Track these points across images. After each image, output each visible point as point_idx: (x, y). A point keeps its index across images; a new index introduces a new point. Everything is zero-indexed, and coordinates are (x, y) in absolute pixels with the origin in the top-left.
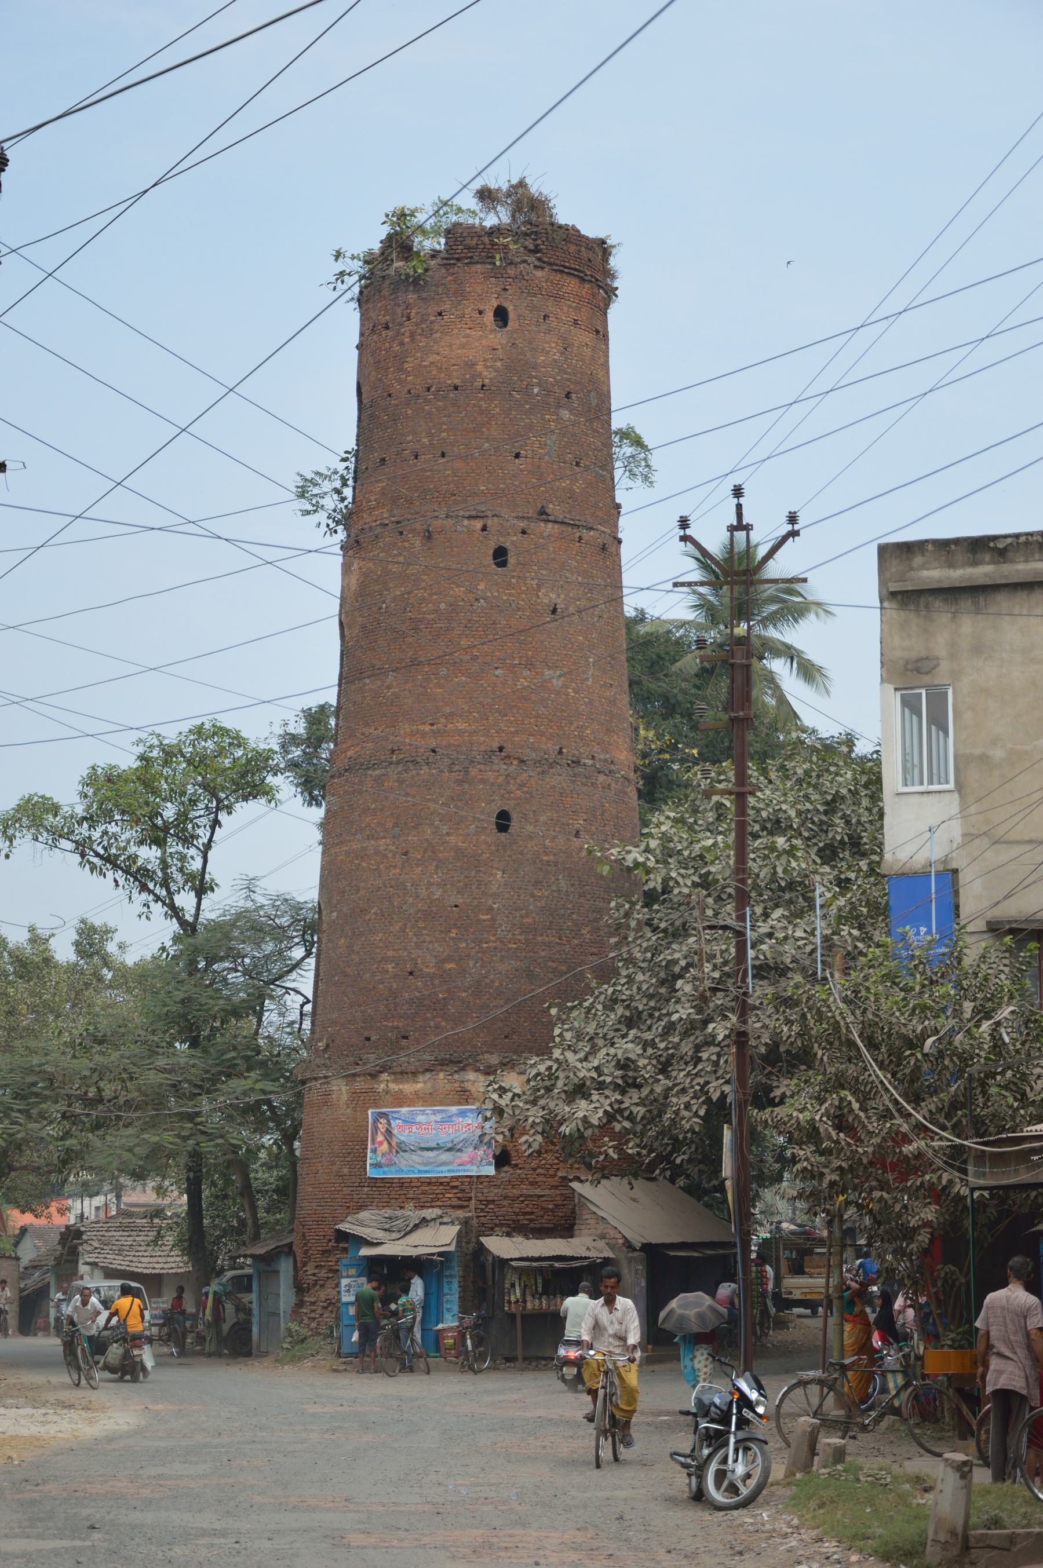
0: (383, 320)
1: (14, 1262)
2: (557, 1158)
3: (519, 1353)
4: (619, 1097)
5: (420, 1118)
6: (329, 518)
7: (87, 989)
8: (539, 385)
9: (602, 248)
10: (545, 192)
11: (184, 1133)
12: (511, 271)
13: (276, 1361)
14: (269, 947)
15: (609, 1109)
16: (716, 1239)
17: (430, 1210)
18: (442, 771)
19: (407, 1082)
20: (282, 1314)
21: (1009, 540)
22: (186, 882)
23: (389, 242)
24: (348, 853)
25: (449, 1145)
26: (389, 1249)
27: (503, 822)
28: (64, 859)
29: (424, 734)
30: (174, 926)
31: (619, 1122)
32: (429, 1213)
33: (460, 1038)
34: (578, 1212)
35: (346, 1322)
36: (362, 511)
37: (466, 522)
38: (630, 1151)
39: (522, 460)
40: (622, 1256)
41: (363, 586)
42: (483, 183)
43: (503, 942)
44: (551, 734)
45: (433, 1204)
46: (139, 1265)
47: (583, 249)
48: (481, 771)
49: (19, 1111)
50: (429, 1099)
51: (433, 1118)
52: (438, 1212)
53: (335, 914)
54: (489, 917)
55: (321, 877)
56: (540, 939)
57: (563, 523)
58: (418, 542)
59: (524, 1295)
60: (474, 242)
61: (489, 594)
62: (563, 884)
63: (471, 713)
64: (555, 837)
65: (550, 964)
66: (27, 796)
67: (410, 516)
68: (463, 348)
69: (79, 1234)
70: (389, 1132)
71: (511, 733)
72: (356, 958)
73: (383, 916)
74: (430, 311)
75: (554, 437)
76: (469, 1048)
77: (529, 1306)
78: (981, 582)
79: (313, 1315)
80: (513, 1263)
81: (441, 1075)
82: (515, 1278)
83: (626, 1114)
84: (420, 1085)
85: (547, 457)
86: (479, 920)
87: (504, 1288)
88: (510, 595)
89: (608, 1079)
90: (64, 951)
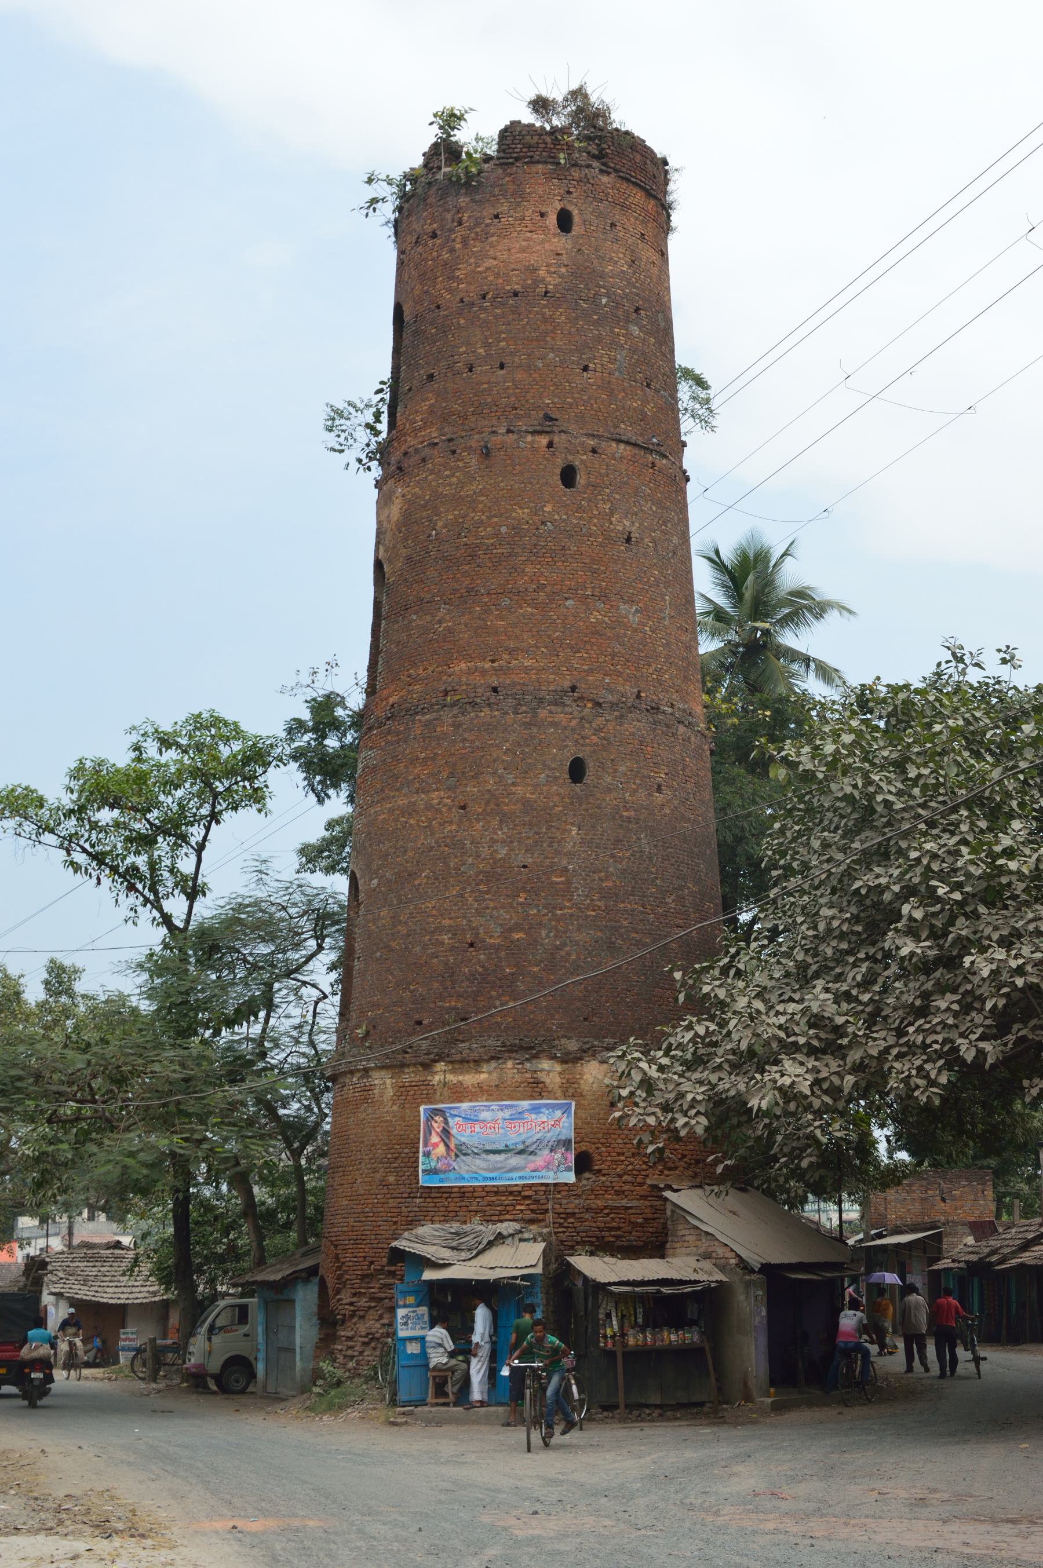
0: (429, 229)
5: (485, 1115)
8: (607, 295)
12: (576, 173)
16: (807, 1259)
17: (506, 1224)
18: (507, 713)
19: (468, 1072)
20: (298, 1350)
22: (176, 885)
24: (391, 811)
25: (521, 1147)
27: (577, 770)
29: (483, 672)
32: (506, 1227)
33: (531, 1020)
34: (670, 1227)
35: (402, 1363)
37: (529, 438)
39: (591, 374)
41: (407, 519)
43: (579, 908)
44: (628, 674)
45: (502, 1218)
46: (105, 1295)
47: (648, 162)
48: (551, 712)
50: (495, 1092)
51: (500, 1115)
52: (514, 1226)
53: (375, 881)
54: (563, 879)
58: (474, 461)
59: (621, 1327)
61: (556, 517)
64: (635, 791)
65: (634, 935)
66: (10, 787)
67: (464, 434)
68: (524, 252)
70: (446, 1133)
71: (585, 671)
73: (436, 879)
75: (624, 353)
77: (631, 1341)
79: (350, 1352)
80: (612, 1288)
81: (510, 1064)
82: (611, 1307)
84: (483, 1076)
85: (617, 373)
86: (552, 882)
89: (802, 1040)
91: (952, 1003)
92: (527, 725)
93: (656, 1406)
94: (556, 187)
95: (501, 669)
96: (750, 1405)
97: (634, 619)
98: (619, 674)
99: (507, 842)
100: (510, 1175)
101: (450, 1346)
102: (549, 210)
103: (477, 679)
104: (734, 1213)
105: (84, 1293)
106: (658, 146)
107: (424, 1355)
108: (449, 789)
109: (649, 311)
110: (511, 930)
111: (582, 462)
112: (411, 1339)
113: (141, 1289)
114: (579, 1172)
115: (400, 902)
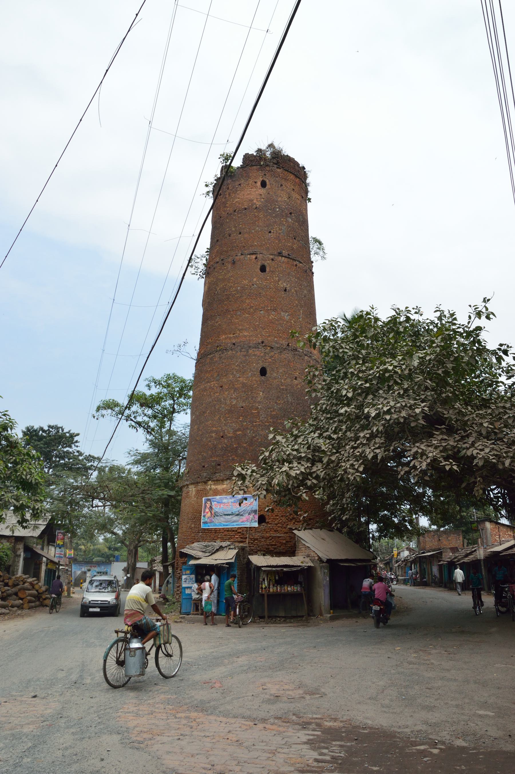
2: (287, 519)
3: (266, 614)
5: (225, 501)
8: (279, 208)
12: (268, 168)
25: (237, 513)
26: (205, 561)
27: (263, 372)
29: (230, 338)
31: (310, 480)
32: (224, 544)
34: (297, 545)
35: (184, 597)
37: (249, 256)
38: (317, 496)
39: (272, 234)
40: (318, 565)
50: (224, 492)
51: (230, 500)
59: (269, 585)
62: (290, 399)
70: (211, 507)
72: (200, 433)
75: (285, 227)
77: (271, 590)
79: (178, 592)
83: (314, 475)
84: (225, 486)
87: (259, 581)
91: (367, 434)
93: (283, 617)
96: (321, 617)
97: (287, 318)
98: (281, 337)
100: (233, 524)
103: (228, 341)
104: (323, 539)
106: (301, 162)
108: (217, 381)
111: (268, 263)
112: (187, 588)
114: (260, 523)
115: (200, 423)
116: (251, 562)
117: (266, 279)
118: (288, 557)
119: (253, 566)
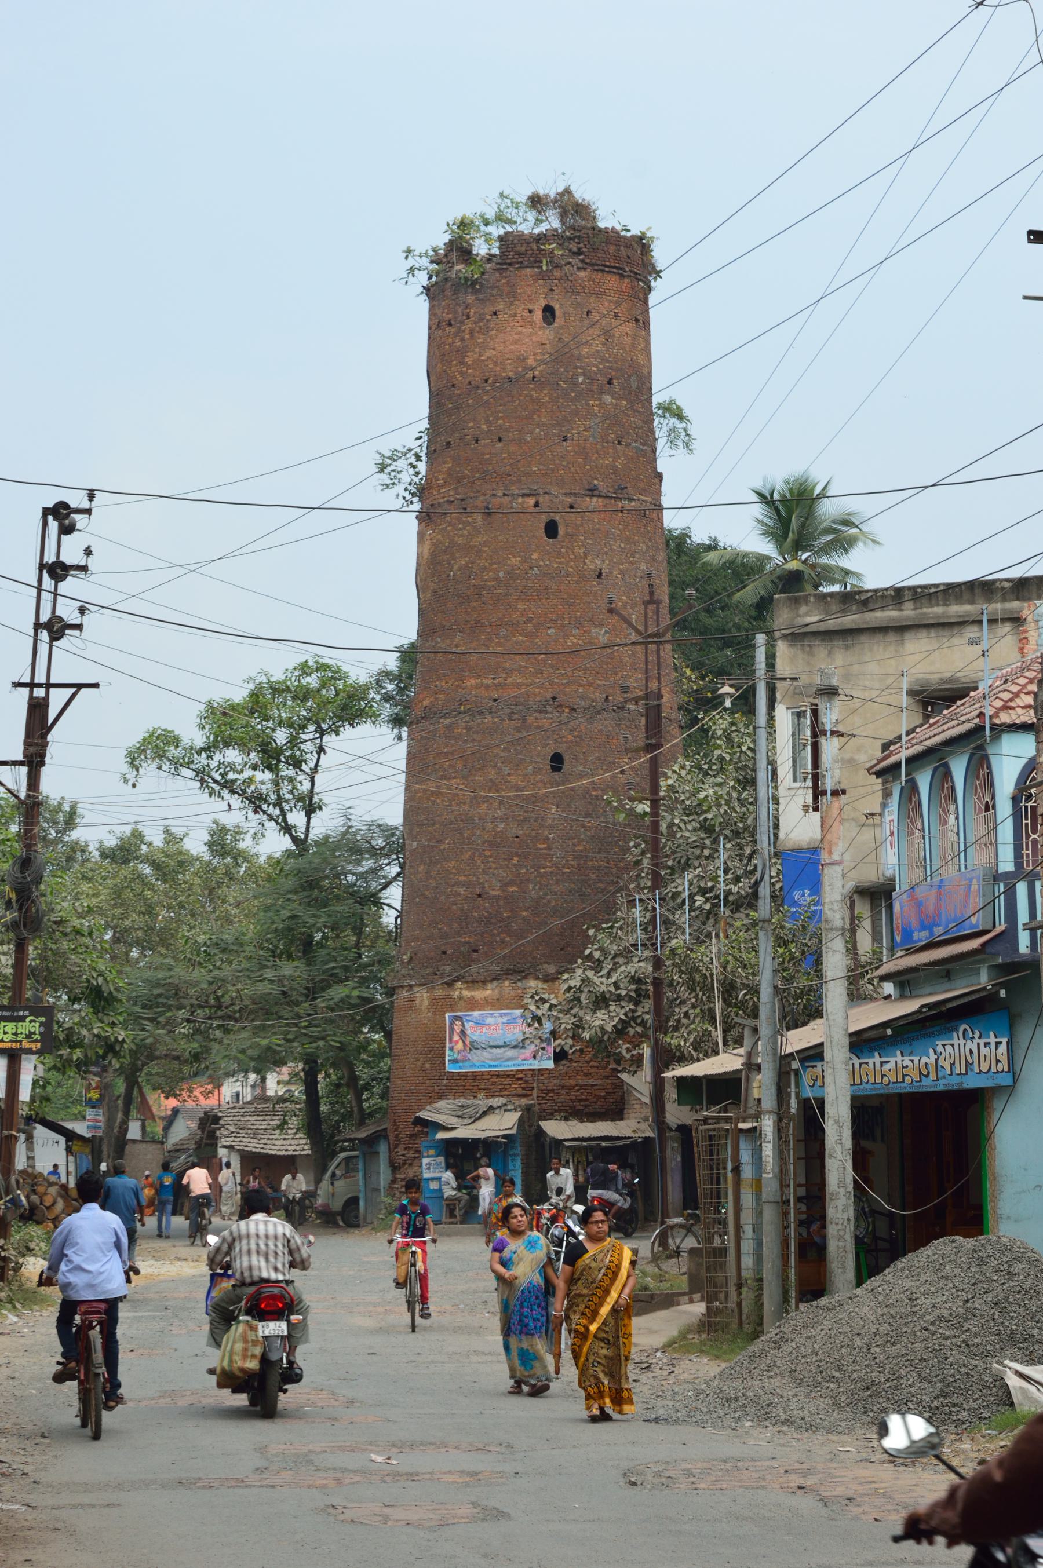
1: (159, 1146)
4: (633, 1007)
6: (406, 489)
7: (219, 887)
8: (584, 374)
9: (642, 244)
10: (587, 198)
11: (290, 1037)
12: (557, 273)
13: (373, 1229)
14: (369, 864)
15: (623, 1017)
21: (870, 594)
23: (451, 245)
24: (425, 791)
25: (514, 1043)
27: (557, 762)
28: (186, 784)
29: (487, 687)
30: (286, 843)
32: (496, 1102)
33: (522, 951)
35: (427, 1195)
36: (431, 488)
37: (520, 500)
41: (434, 555)
42: (533, 190)
47: (622, 248)
49: (148, 1019)
50: (496, 1004)
51: (500, 1020)
52: (503, 1100)
55: (405, 810)
56: (590, 863)
57: (606, 497)
58: (479, 518)
60: (523, 249)
61: (541, 563)
63: (527, 668)
65: (600, 885)
67: (472, 495)
69: (216, 1119)
70: (463, 1033)
74: (486, 310)
76: (530, 959)
78: (848, 626)
81: (507, 983)
82: (569, 1157)
83: (639, 1021)
84: (489, 992)
88: (560, 563)
89: (623, 993)
90: (196, 845)
92: (518, 730)
94: (541, 287)
95: (500, 684)
98: (590, 685)
99: (505, 819)
101: (454, 1184)
102: (536, 307)
105: (254, 1146)
107: (440, 1190)
108: (463, 777)
109: (633, 380)
110: (508, 884)
112: (433, 1179)
113: (293, 1143)
116: (544, 1132)
117: (560, 555)
118: (609, 1123)
119: (548, 1140)
